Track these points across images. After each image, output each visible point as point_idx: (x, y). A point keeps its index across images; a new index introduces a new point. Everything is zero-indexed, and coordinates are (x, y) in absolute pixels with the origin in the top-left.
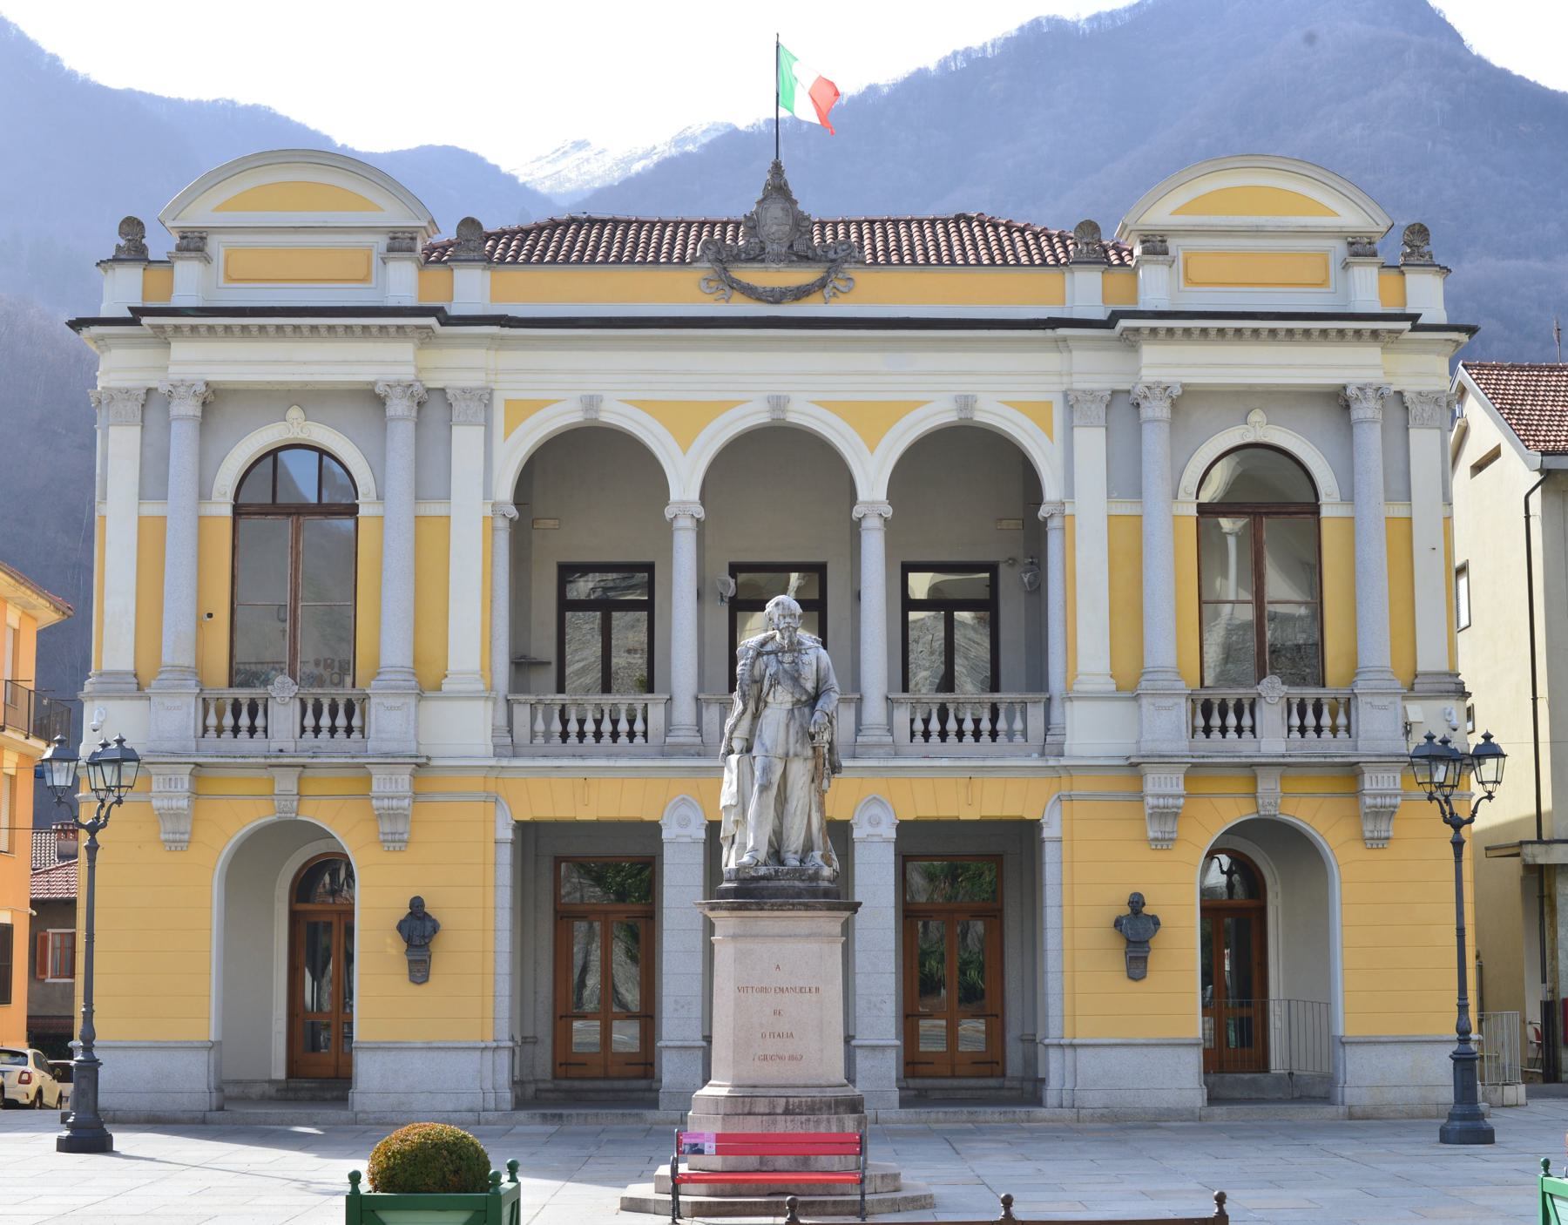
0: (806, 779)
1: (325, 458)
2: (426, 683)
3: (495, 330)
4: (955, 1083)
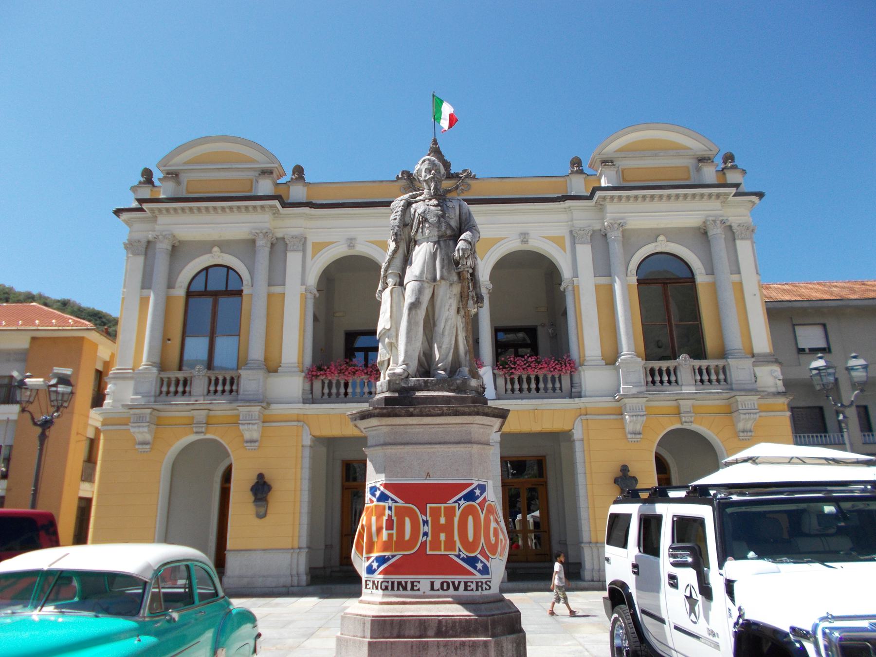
0: (453, 303)
2: (271, 367)
3: (307, 210)
4: (529, 565)
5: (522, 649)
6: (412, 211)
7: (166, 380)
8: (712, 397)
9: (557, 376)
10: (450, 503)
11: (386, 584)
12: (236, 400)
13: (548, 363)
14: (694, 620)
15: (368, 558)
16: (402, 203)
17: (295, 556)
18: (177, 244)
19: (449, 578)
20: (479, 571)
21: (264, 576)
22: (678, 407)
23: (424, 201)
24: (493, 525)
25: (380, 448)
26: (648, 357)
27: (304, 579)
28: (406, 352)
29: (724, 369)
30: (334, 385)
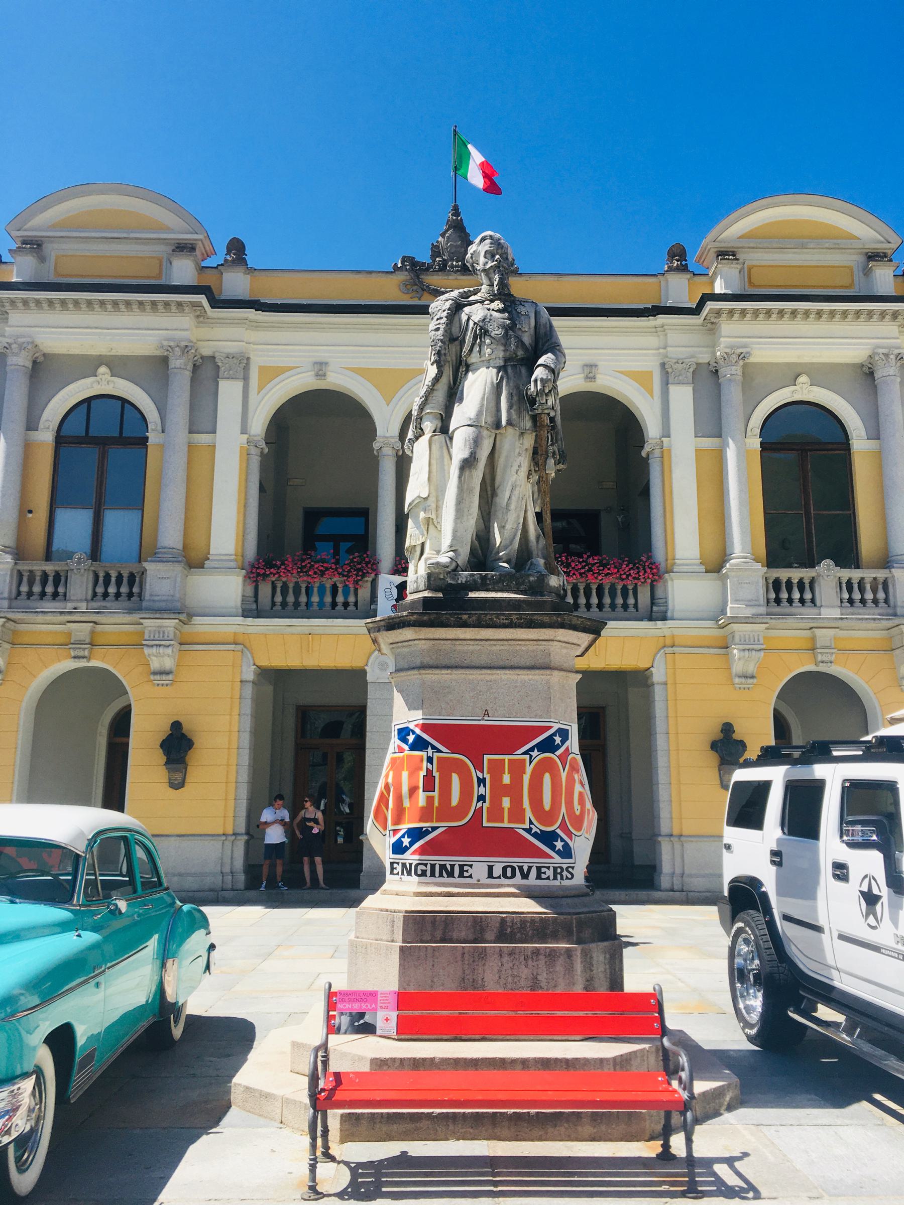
0: (524, 462)
1: (126, 405)
2: (194, 560)
3: (251, 313)
5: (617, 962)
6: (464, 318)
7: (26, 574)
8: (866, 628)
9: (630, 587)
10: (518, 755)
11: (424, 868)
12: (140, 609)
13: (618, 568)
14: (874, 923)
15: (395, 831)
16: (448, 304)
17: (228, 844)
18: (41, 359)
19: (515, 861)
20: (559, 853)
21: (180, 875)
22: (813, 639)
23: (482, 302)
24: (578, 788)
25: (416, 672)
26: (772, 561)
27: (241, 878)
28: (455, 532)
29: (885, 584)
30: (291, 591)
